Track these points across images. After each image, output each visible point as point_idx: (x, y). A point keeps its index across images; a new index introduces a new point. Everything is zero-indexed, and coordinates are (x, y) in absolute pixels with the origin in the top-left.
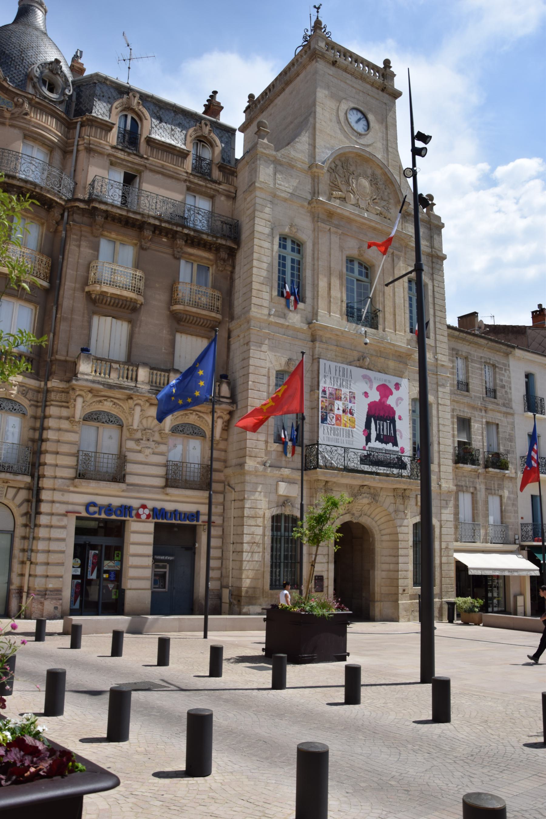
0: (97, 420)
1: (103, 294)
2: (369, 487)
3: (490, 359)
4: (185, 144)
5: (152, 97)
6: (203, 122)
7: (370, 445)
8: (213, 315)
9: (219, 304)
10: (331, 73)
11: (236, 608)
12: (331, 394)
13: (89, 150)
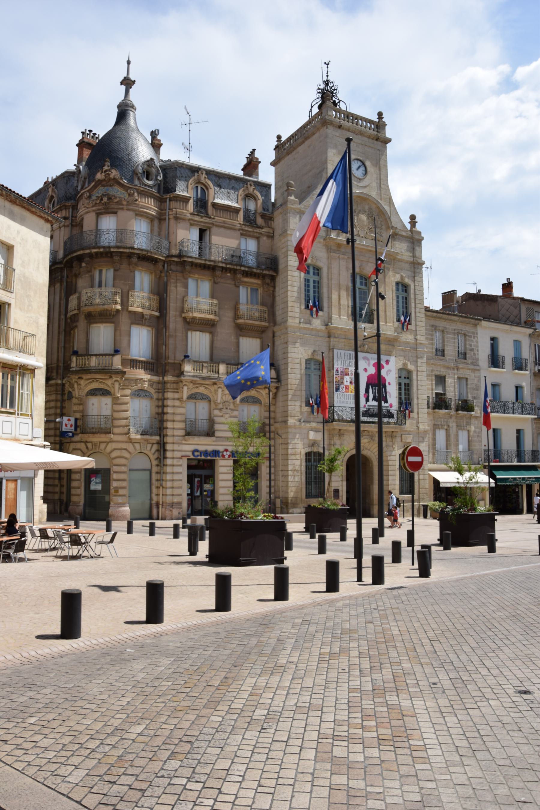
0: (195, 398)
1: (194, 318)
2: (368, 432)
4: (237, 202)
6: (249, 183)
7: (368, 403)
8: (263, 323)
9: (266, 315)
10: (337, 134)
11: (285, 510)
12: (342, 372)
13: (177, 218)
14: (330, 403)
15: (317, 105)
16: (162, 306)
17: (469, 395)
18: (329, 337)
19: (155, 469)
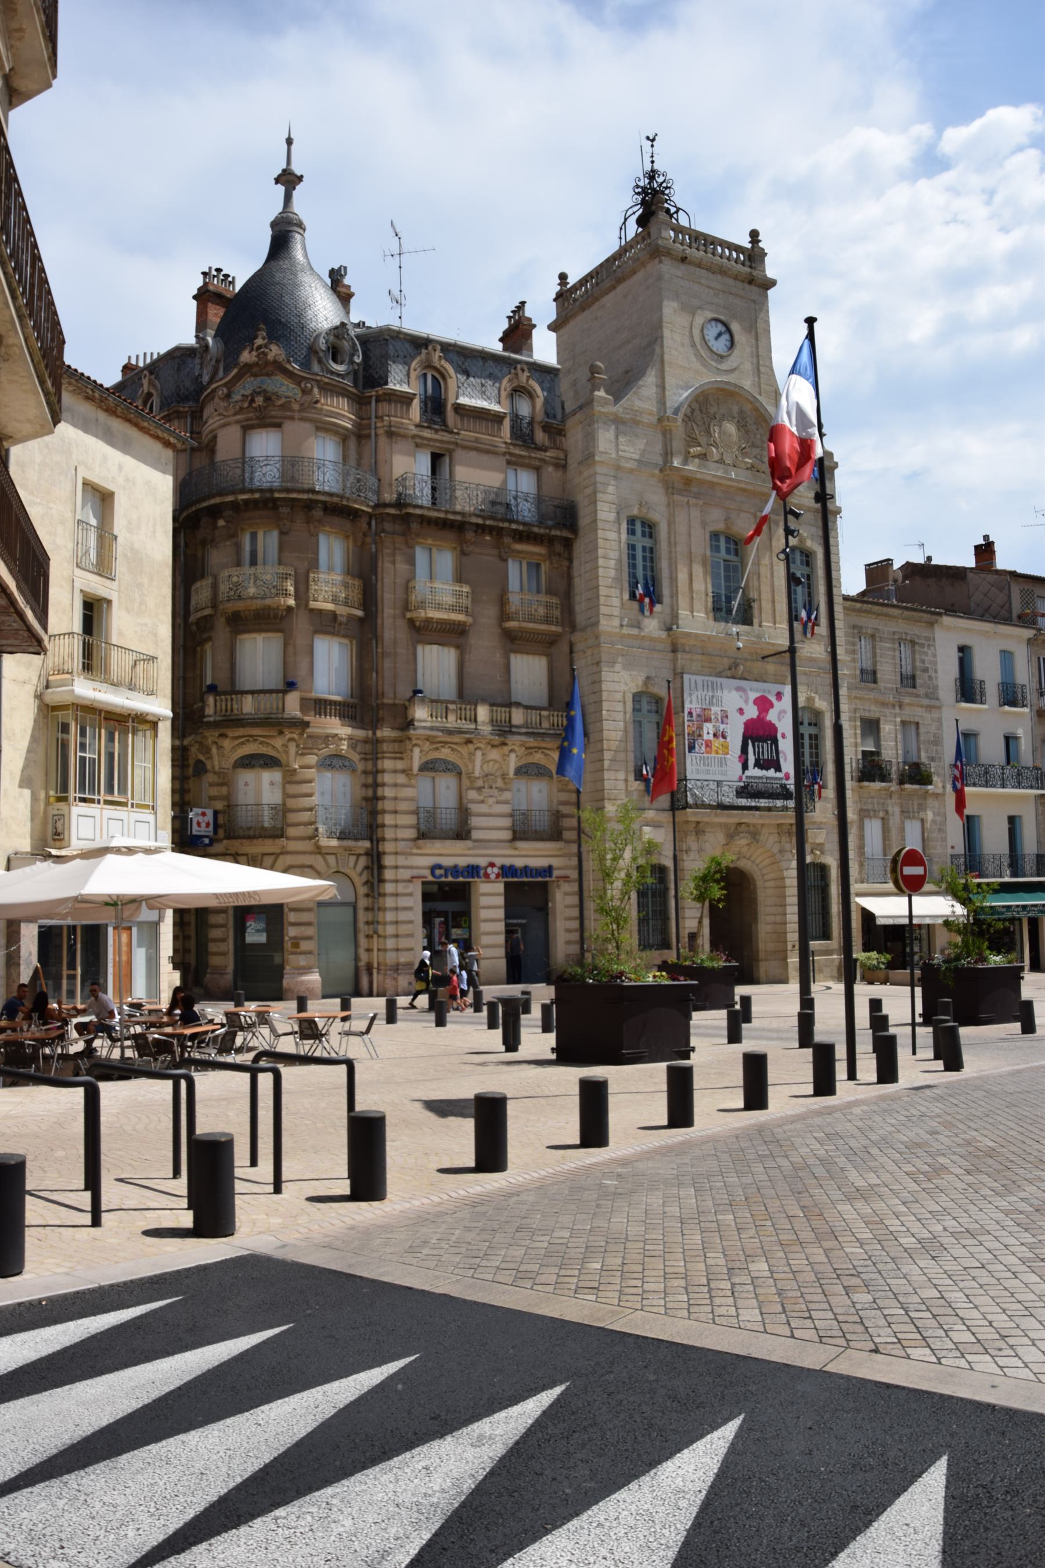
0: (433, 769)
1: (428, 621)
2: (748, 825)
3: (906, 634)
4: (499, 403)
5: (455, 345)
6: (519, 366)
7: (747, 773)
8: (553, 628)
9: (557, 613)
10: (679, 274)
12: (699, 716)
13: (391, 434)
14: (679, 773)
16: (369, 599)
17: (923, 754)
18: (674, 650)
19: (362, 903)
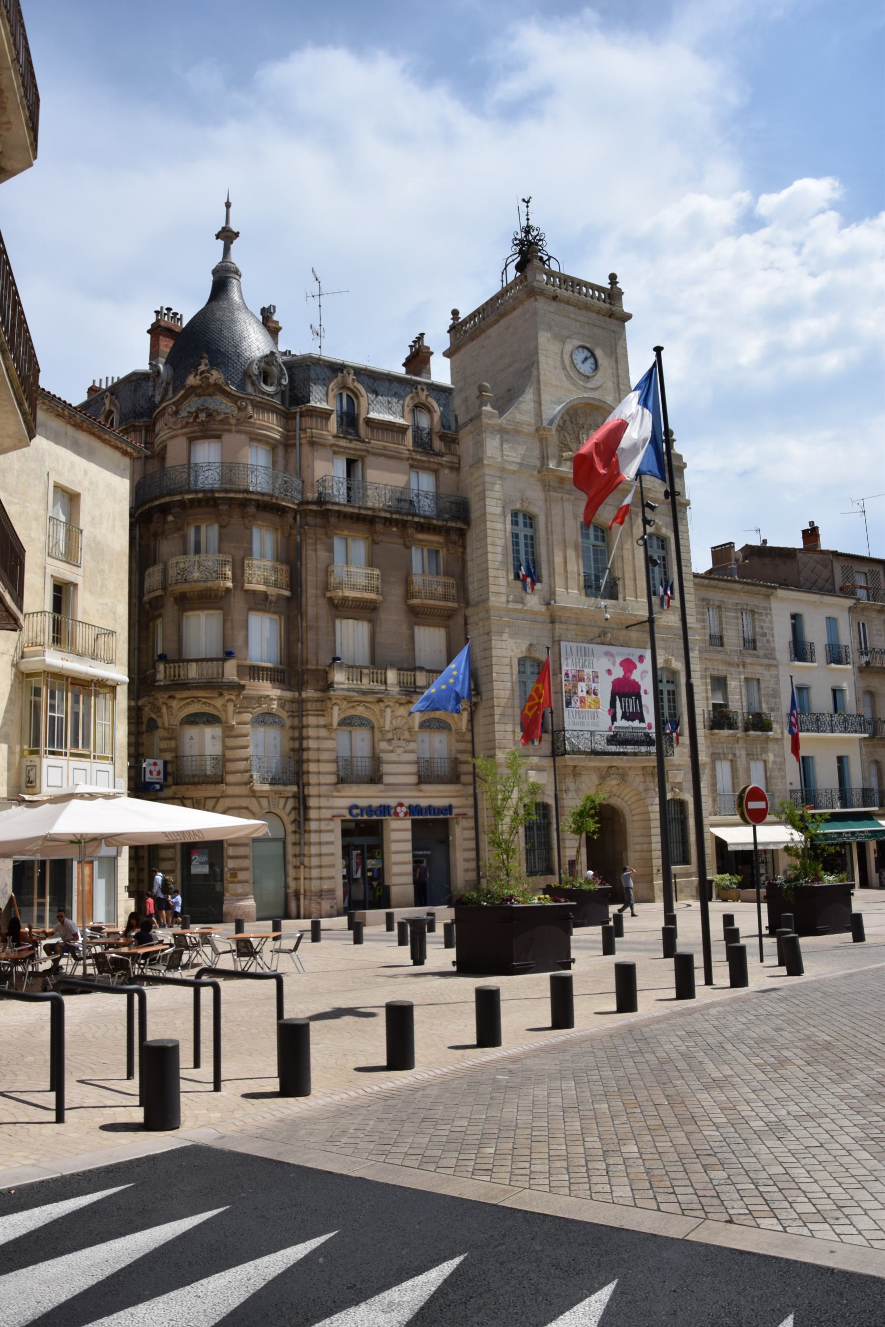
0: (350, 724)
1: (345, 599)
2: (617, 768)
3: (747, 605)
4: (403, 417)
6: (419, 387)
7: (616, 724)
8: (450, 604)
9: (453, 591)
10: (552, 310)
13: (312, 444)
15: (514, 264)
16: (295, 581)
17: (764, 706)
18: (553, 622)
